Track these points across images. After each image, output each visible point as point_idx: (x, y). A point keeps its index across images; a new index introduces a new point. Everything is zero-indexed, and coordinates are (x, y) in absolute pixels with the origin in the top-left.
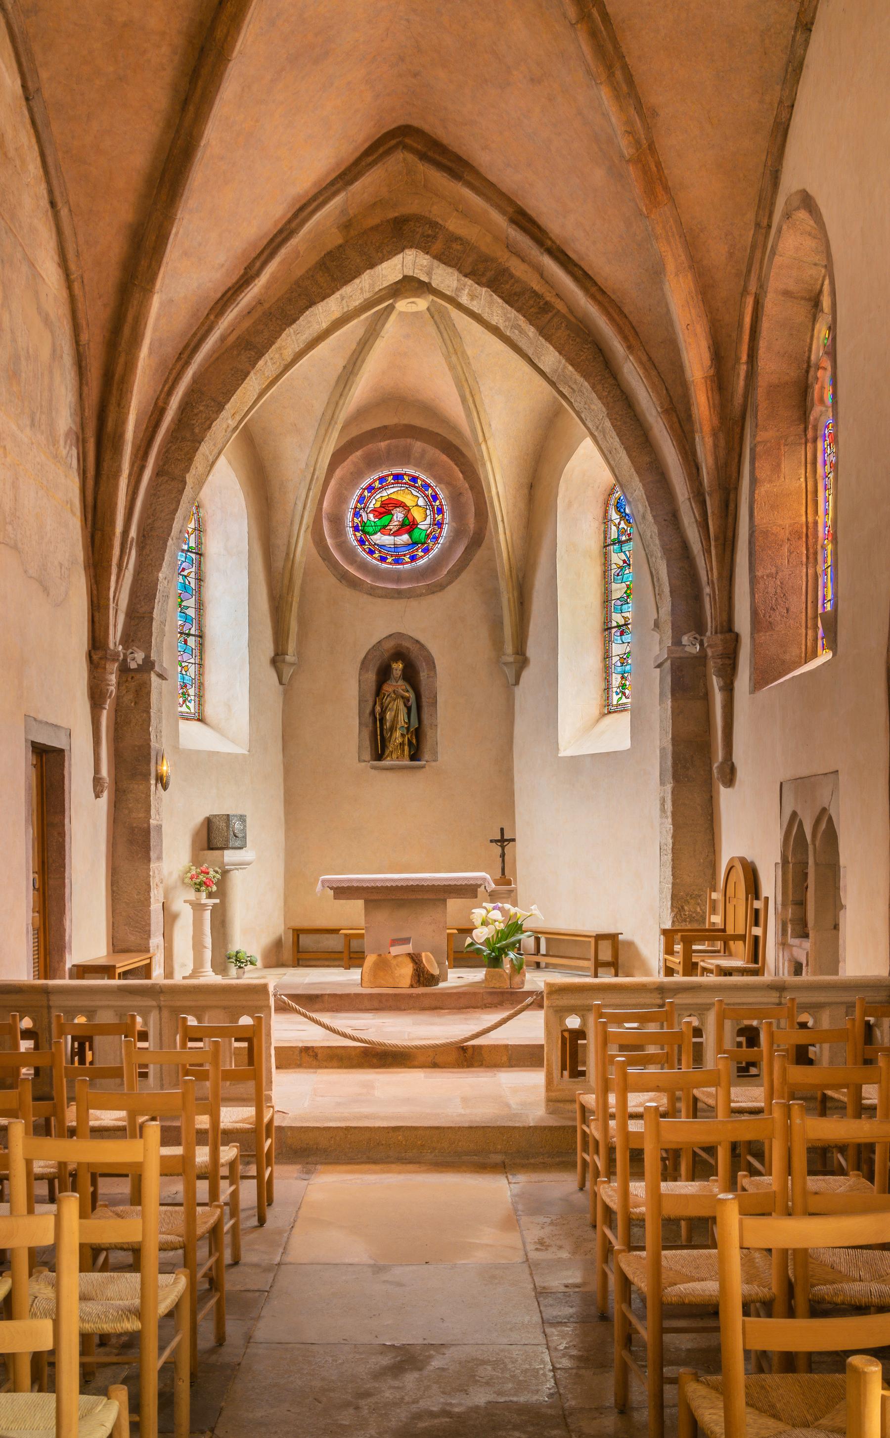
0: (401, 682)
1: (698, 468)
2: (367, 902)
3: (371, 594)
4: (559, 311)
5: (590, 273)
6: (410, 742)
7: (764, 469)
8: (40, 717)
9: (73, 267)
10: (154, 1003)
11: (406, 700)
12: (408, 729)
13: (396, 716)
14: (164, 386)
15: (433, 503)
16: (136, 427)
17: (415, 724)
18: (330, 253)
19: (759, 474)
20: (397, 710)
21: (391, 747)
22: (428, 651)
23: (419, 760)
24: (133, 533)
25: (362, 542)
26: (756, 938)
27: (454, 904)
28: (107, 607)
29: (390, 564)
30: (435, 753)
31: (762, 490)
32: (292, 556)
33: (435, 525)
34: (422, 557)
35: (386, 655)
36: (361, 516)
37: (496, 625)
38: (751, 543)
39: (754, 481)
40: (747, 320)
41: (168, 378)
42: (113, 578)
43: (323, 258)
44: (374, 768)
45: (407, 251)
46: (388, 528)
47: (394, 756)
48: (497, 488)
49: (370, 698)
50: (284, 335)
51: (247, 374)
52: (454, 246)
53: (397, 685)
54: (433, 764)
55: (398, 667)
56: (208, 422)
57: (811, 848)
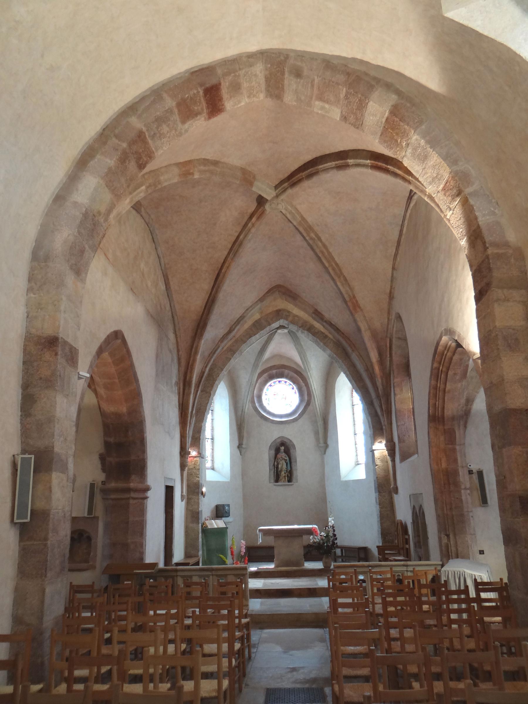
0: (284, 454)
1: (378, 388)
2: (275, 537)
3: (272, 423)
4: (330, 338)
5: (339, 328)
6: (288, 476)
7: (397, 390)
8: (168, 477)
9: (177, 333)
10: (211, 573)
11: (286, 460)
12: (287, 471)
13: (282, 466)
14: (204, 365)
16: (196, 377)
17: (289, 469)
18: (256, 321)
19: (396, 392)
20: (283, 464)
21: (281, 478)
22: (293, 443)
23: (291, 482)
24: (194, 412)
26: (407, 549)
27: (305, 537)
28: (186, 437)
30: (297, 480)
31: (398, 397)
32: (244, 411)
35: (278, 445)
37: (317, 433)
38: (396, 412)
39: (395, 394)
40: (388, 345)
41: (205, 362)
43: (254, 322)
44: (275, 485)
45: (281, 320)
47: (282, 481)
48: (314, 386)
50: (242, 347)
51: (230, 359)
52: (296, 318)
53: (282, 455)
54: (297, 483)
55: (282, 448)
56: (218, 375)
57: (419, 517)
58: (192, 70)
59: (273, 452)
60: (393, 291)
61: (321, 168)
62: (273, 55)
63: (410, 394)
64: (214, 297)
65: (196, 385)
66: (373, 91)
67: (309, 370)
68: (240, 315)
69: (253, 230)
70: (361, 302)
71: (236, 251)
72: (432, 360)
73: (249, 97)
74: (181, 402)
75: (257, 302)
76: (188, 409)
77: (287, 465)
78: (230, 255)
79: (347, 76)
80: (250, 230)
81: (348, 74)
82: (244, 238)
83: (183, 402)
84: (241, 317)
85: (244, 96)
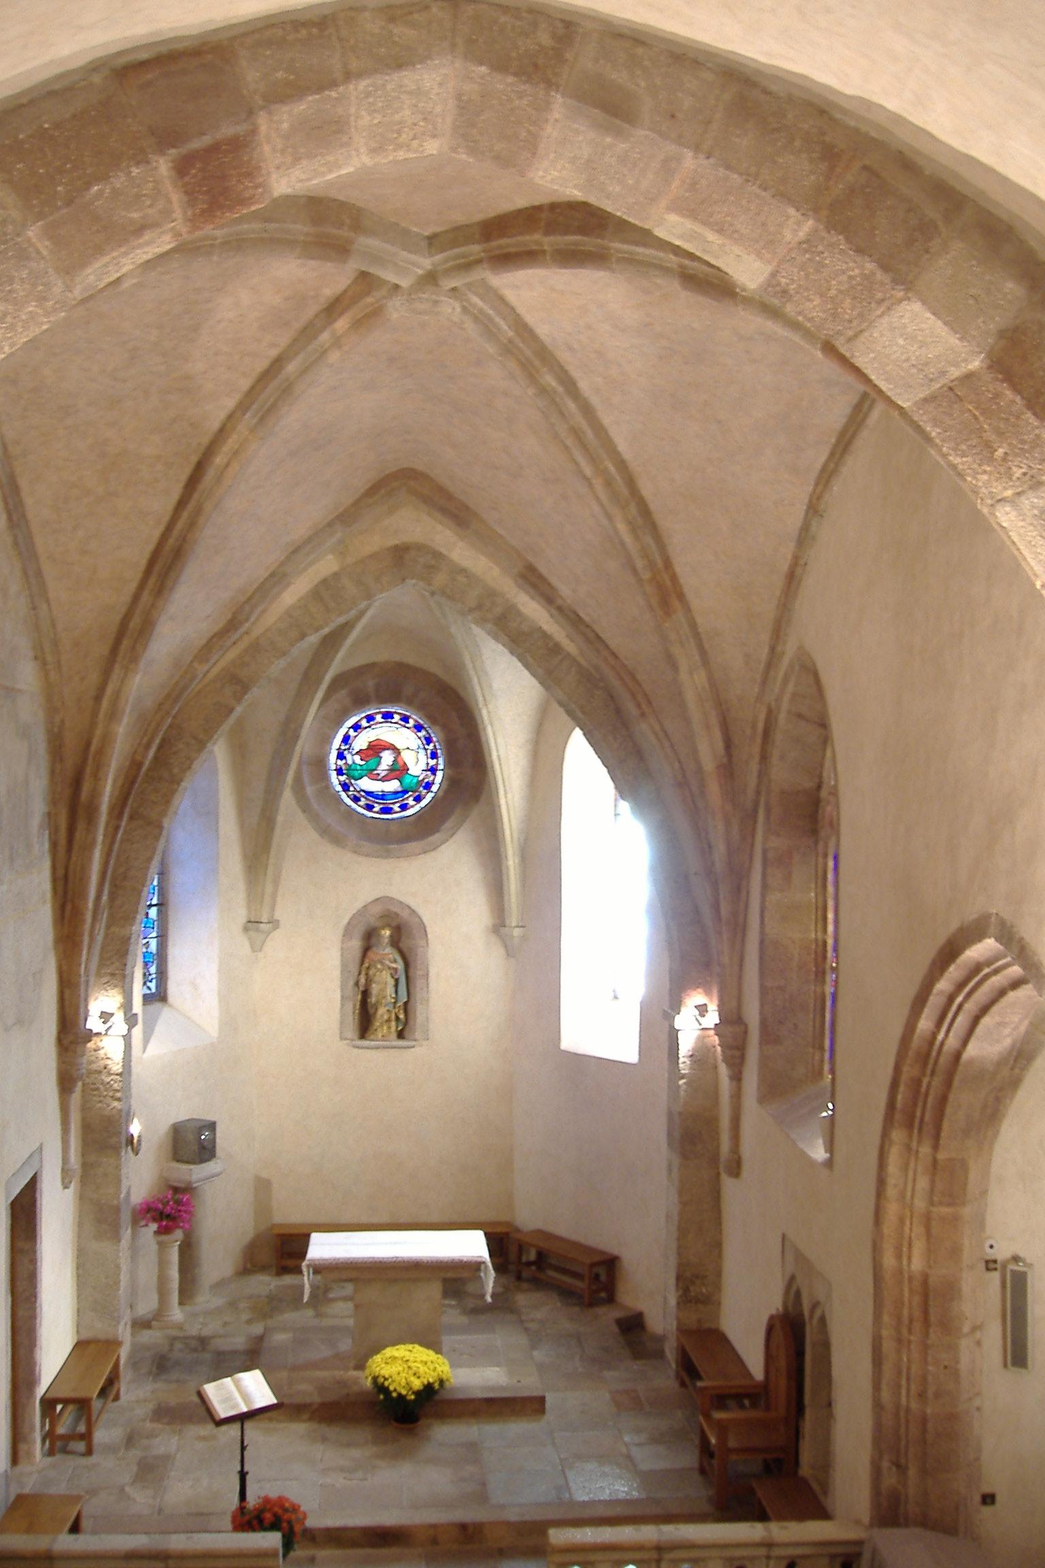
0: (389, 950)
4: (568, 654)
6: (397, 1018)
13: (383, 990)
15: (426, 747)
17: (403, 998)
18: (324, 581)
25: (345, 787)
29: (377, 813)
30: (426, 1031)
33: (429, 770)
34: (412, 806)
36: (345, 758)
42: (85, 952)
46: (376, 772)
49: (354, 968)
58: (123, 61)
59: (356, 944)
60: (799, 570)
61: (618, 251)
62: (503, 19)
63: (813, 894)
64: (184, 540)
65: (112, 809)
66: (927, 251)
67: (485, 700)
68: (272, 569)
69: (334, 357)
70: (689, 581)
71: (266, 407)
72: (934, 963)
73: (373, 151)
74: (61, 872)
75: (330, 525)
76: (83, 894)
77: (396, 986)
78: (246, 417)
79: (823, 166)
80: (323, 353)
81: (830, 155)
82: (304, 371)
83: (67, 868)
84: (272, 575)
85: (357, 150)
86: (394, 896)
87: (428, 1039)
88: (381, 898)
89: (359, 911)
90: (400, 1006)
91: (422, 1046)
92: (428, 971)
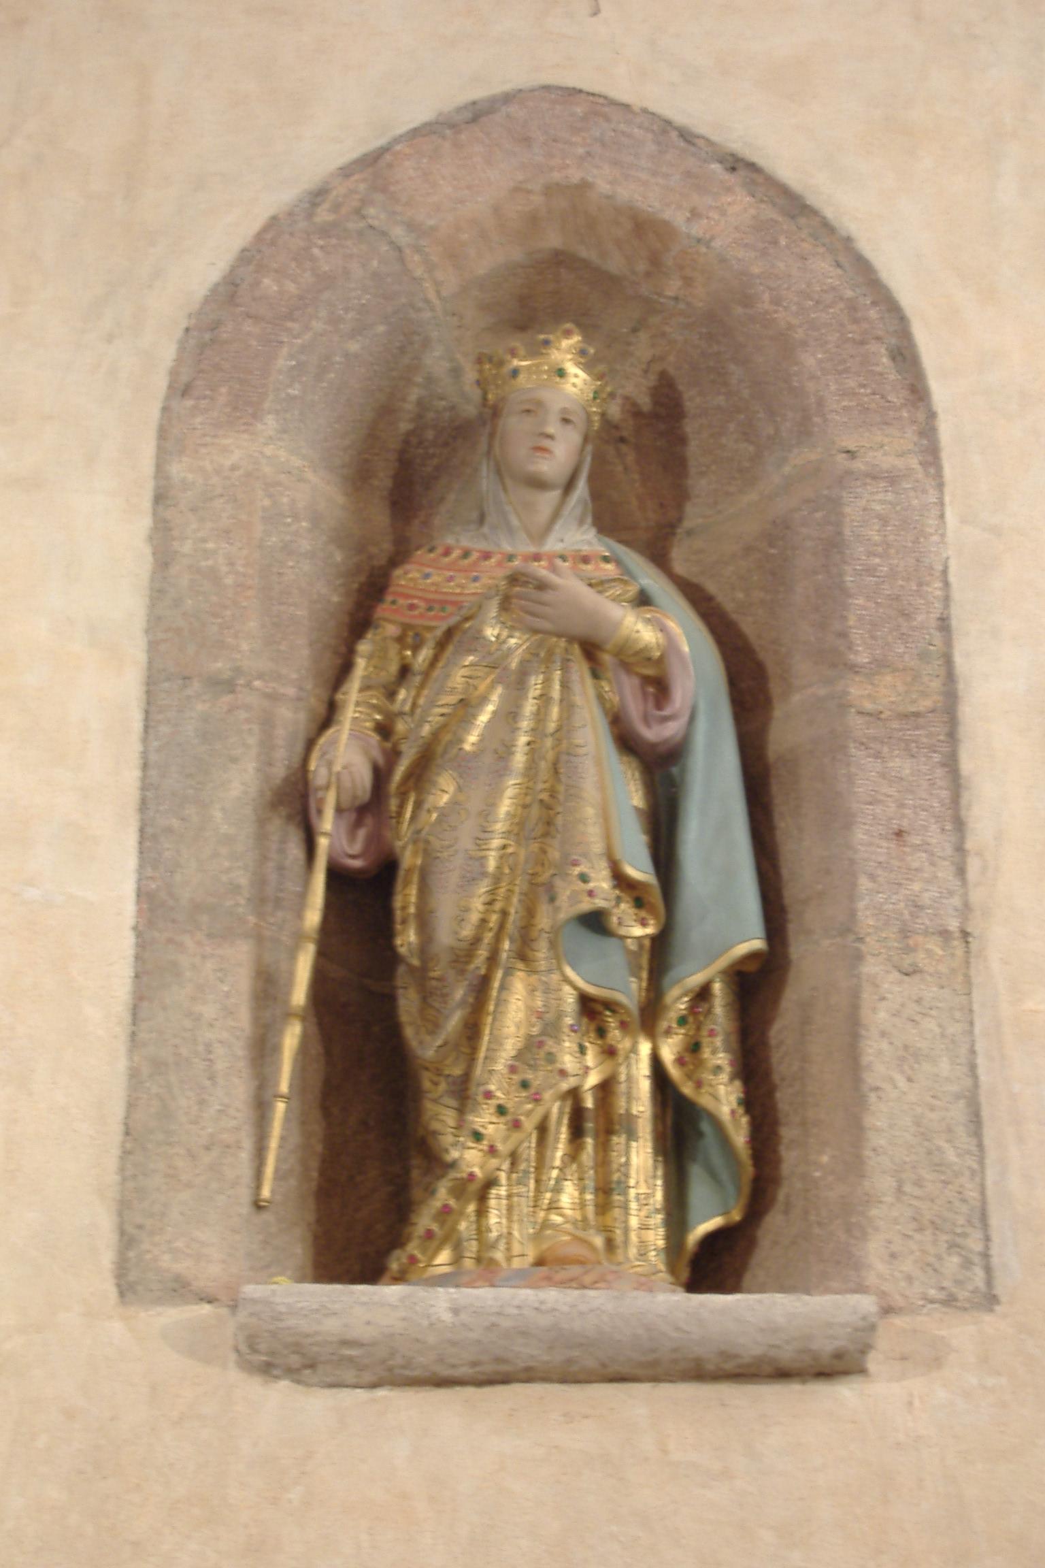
86: (622, 90)
87: (990, 1300)
88: (508, 98)
89: (318, 195)
90: (703, 994)
91: (935, 1361)
92: (950, 676)
